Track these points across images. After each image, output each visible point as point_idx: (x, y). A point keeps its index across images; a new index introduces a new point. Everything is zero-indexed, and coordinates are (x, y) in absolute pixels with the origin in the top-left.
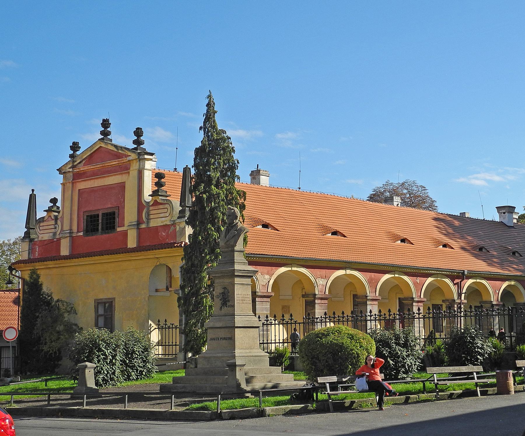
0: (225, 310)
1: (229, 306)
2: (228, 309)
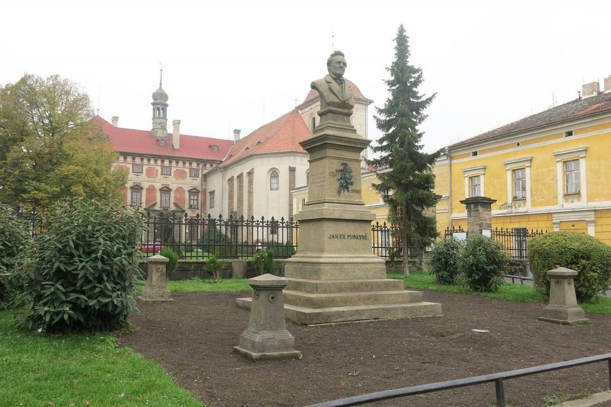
0: (345, 196)
1: (353, 191)
2: (351, 194)
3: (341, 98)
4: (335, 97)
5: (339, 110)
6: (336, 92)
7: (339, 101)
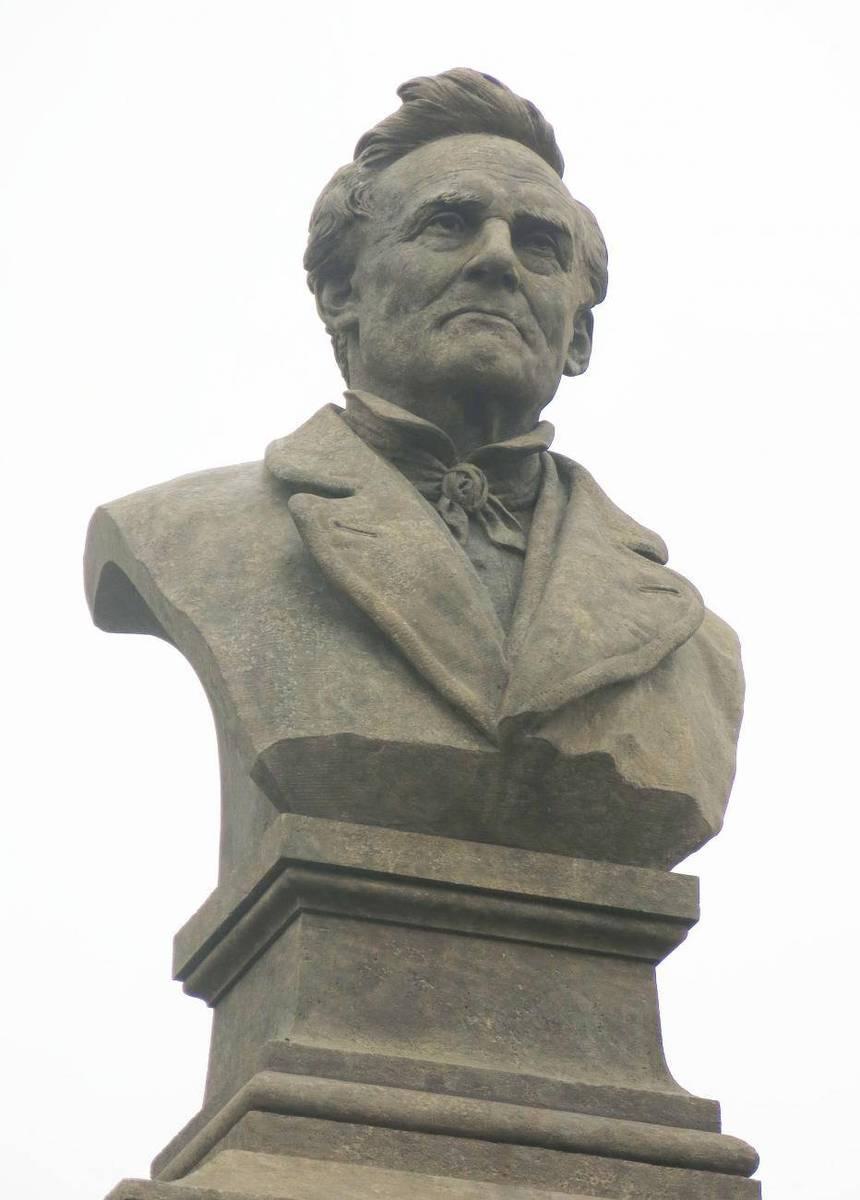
3: (465, 690)
4: (379, 682)
5: (460, 862)
6: (388, 607)
7: (435, 731)
